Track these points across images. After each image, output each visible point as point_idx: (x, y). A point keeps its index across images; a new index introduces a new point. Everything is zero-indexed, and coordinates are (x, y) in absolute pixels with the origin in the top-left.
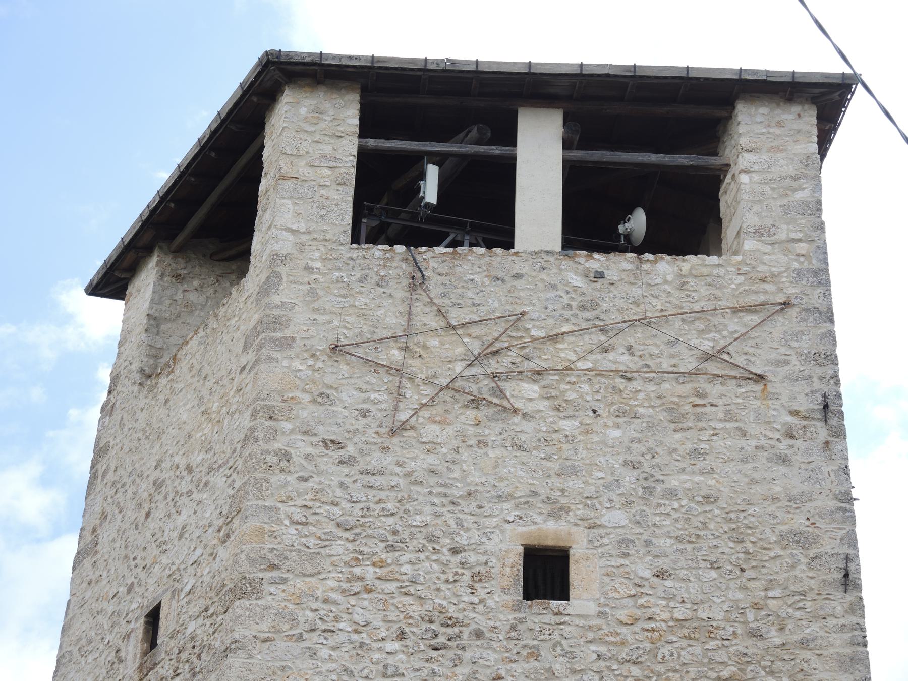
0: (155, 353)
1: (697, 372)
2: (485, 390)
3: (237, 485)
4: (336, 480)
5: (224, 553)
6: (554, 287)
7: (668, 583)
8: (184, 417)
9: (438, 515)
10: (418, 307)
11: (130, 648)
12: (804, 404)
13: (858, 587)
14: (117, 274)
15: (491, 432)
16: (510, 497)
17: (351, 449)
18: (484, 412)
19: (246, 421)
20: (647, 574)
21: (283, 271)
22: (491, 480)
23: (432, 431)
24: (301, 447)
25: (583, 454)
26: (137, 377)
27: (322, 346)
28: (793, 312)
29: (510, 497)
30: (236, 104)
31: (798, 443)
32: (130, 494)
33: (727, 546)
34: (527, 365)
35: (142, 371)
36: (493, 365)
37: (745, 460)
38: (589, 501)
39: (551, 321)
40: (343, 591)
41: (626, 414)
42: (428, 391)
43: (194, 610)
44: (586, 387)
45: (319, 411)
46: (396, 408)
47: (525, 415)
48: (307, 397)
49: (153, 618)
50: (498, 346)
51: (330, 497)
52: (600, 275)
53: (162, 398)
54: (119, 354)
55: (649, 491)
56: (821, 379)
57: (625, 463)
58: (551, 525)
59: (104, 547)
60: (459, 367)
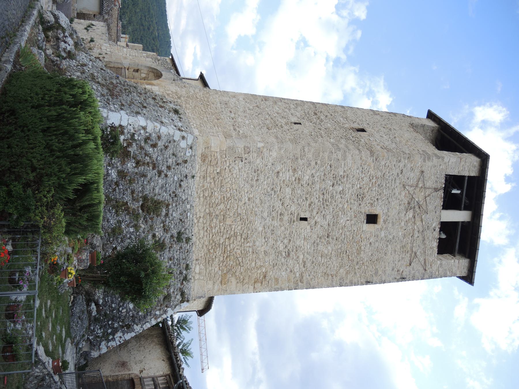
0: (416, 126)
1: (412, 251)
2: (411, 205)
3: (393, 150)
4: (394, 173)
5: (379, 147)
6: (433, 220)
7: (369, 245)
8: (406, 135)
9: (385, 195)
10: (430, 190)
11: (356, 125)
12: (404, 273)
13: (366, 284)
14: (433, 117)
15: (402, 207)
16: (388, 211)
17: (400, 176)
18: (406, 205)
19: (407, 152)
20: (371, 241)
21: (440, 160)
22: (392, 207)
23: (403, 194)
24: (401, 165)
25: (397, 227)
26: (412, 123)
27: (423, 169)
28: (424, 271)
29: (388, 211)
30: (476, 147)
31: (396, 272)
32: (387, 122)
33: (376, 258)
34: (416, 214)
35: (413, 124)
36: (417, 207)
37: (393, 261)
38: (386, 228)
39: (425, 220)
40: (370, 175)
41: (404, 236)
42: (412, 193)
43: (366, 140)
44: (411, 227)
45: (409, 169)
46: (409, 186)
47: (405, 214)
48: (412, 166)
49: (363, 130)
50: (421, 208)
51: (390, 172)
52: (435, 230)
53: (408, 129)
54: (415, 118)
55: (388, 241)
56: (409, 277)
57: (394, 236)
58: (382, 220)
59: (376, 117)
60: (417, 199)
